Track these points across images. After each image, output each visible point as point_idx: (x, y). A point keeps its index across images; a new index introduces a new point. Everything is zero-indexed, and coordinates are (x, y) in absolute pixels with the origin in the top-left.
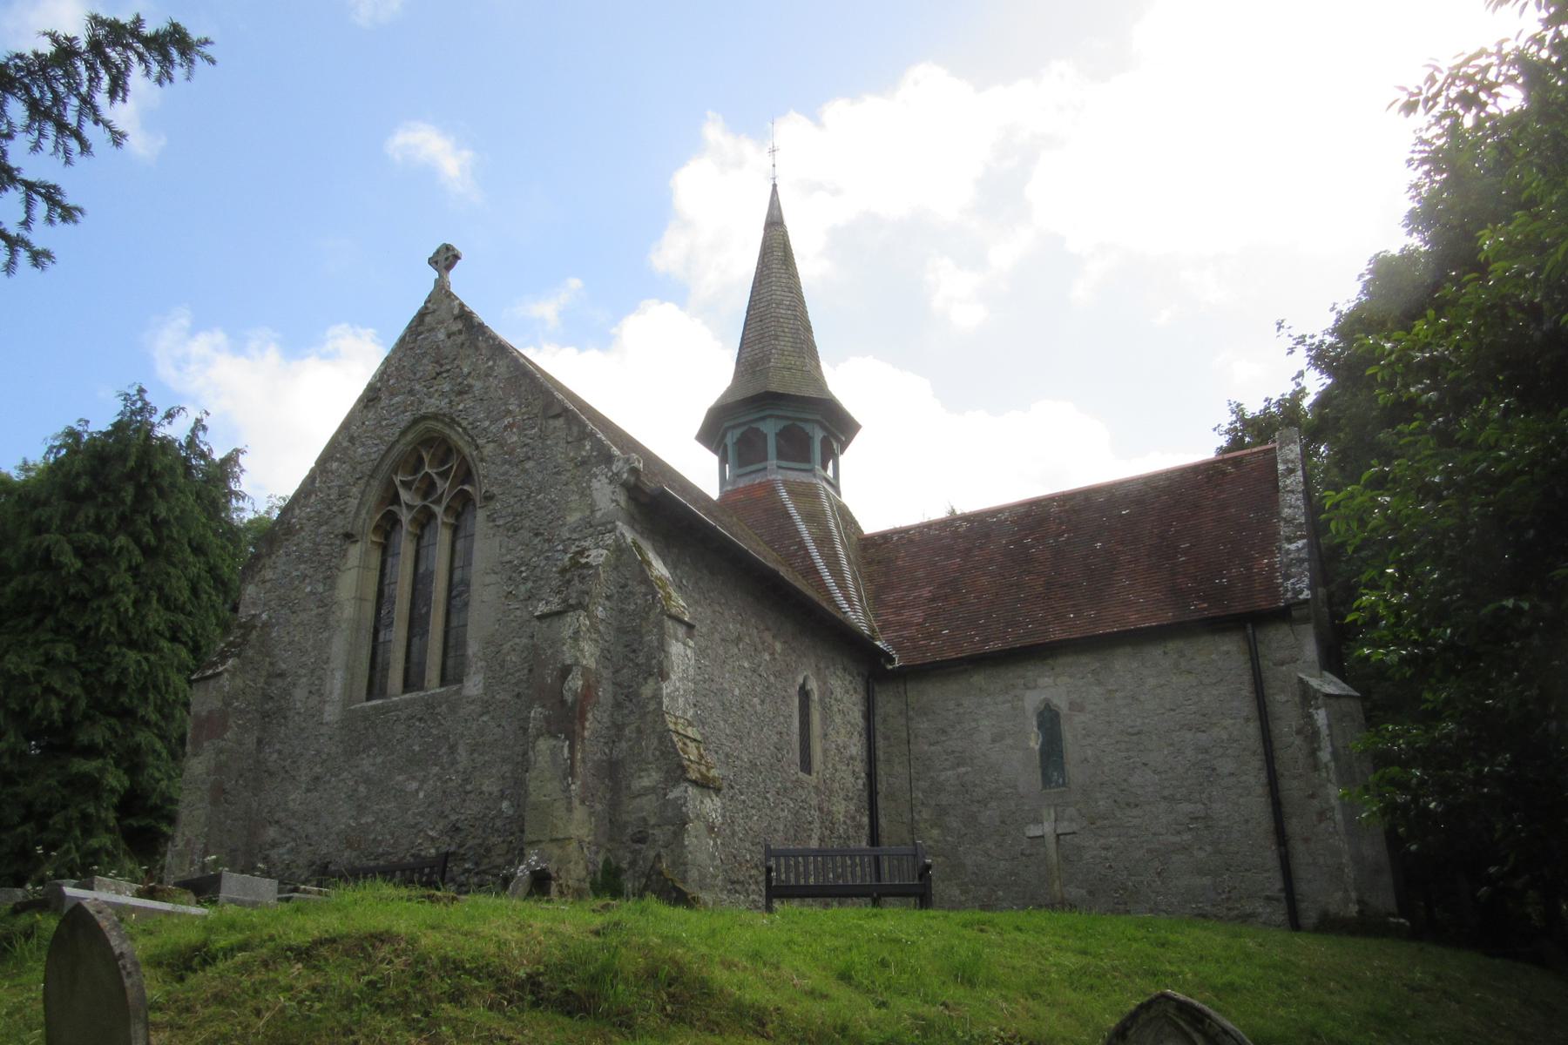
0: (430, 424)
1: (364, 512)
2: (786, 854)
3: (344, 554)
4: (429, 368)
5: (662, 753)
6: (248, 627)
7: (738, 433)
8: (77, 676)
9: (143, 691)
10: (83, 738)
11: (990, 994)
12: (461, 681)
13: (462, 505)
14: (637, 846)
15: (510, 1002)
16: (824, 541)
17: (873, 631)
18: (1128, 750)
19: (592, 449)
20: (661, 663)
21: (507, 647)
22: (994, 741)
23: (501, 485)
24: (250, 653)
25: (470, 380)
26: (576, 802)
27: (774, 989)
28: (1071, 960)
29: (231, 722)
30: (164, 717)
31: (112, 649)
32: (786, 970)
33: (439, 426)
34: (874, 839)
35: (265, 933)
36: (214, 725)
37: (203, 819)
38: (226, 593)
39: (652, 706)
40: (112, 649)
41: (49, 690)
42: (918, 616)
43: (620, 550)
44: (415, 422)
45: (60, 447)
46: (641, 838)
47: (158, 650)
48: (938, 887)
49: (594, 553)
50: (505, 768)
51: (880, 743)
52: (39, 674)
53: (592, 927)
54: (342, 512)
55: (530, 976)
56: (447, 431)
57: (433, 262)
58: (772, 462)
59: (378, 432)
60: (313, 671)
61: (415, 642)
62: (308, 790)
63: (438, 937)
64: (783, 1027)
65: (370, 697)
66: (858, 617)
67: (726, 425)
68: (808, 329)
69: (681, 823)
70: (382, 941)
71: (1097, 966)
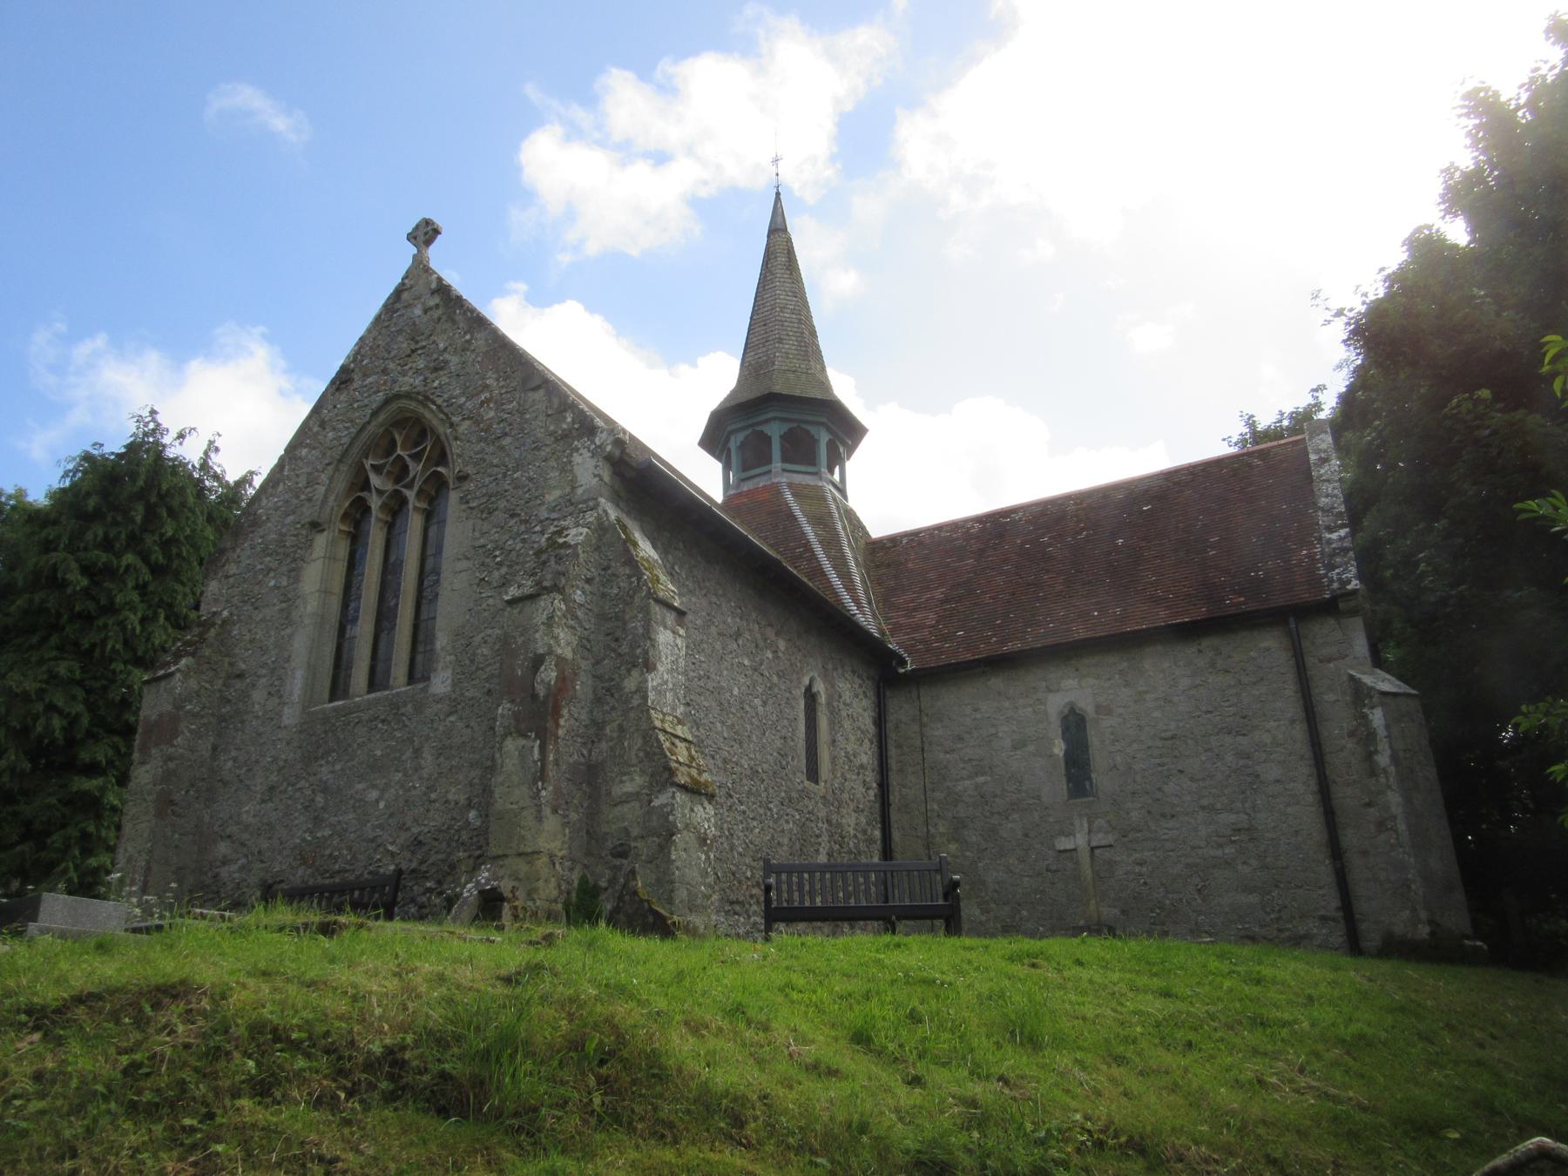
1: (332, 498)
2: (790, 870)
3: (309, 544)
4: (404, 345)
5: (647, 754)
6: (206, 625)
7: (741, 437)
8: (80, 694)
10: (85, 756)
11: (1064, 1060)
12: (428, 679)
13: (435, 489)
14: (617, 862)
15: (350, 1094)
16: (831, 542)
17: (883, 634)
18: (1161, 756)
19: (573, 422)
20: (646, 653)
21: (478, 639)
22: (1015, 748)
23: (476, 464)
24: (207, 652)
25: (447, 356)
26: (547, 811)
27: (760, 1062)
28: (1155, 1007)
29: (183, 726)
31: (118, 666)
32: (780, 1032)
33: (413, 405)
34: (887, 853)
39: (636, 702)
40: (118, 666)
41: (51, 708)
42: (931, 618)
43: (602, 528)
44: (387, 402)
45: (75, 471)
48: (970, 910)
50: (473, 774)
51: (893, 752)
52: (41, 693)
53: (503, 972)
54: (310, 500)
55: (389, 1051)
56: (421, 410)
57: (412, 237)
60: (273, 671)
61: (381, 634)
62: (263, 801)
64: (771, 1128)
66: (867, 619)
67: (729, 428)
68: (813, 334)
69: (667, 834)
70: (175, 997)
71: (1189, 1014)
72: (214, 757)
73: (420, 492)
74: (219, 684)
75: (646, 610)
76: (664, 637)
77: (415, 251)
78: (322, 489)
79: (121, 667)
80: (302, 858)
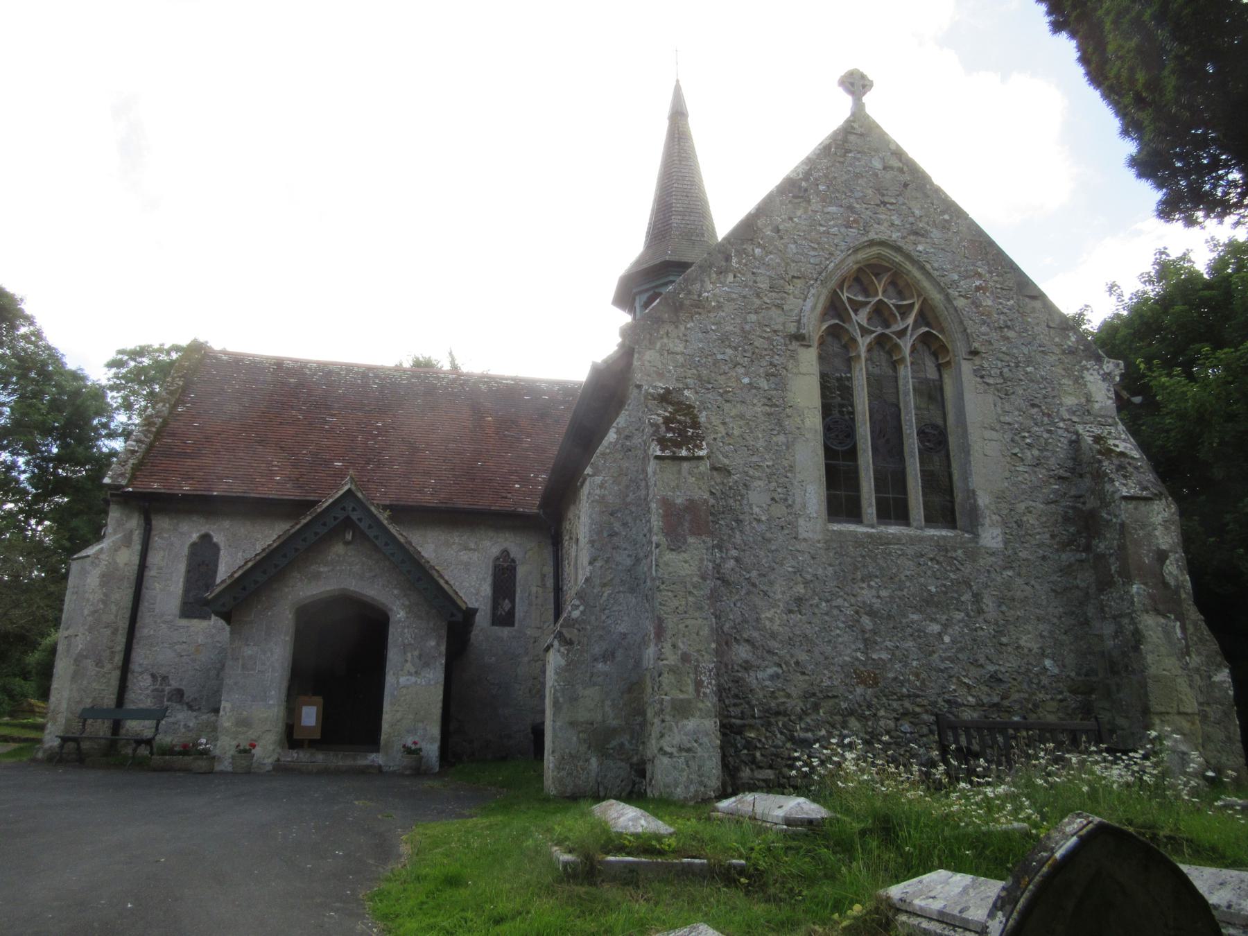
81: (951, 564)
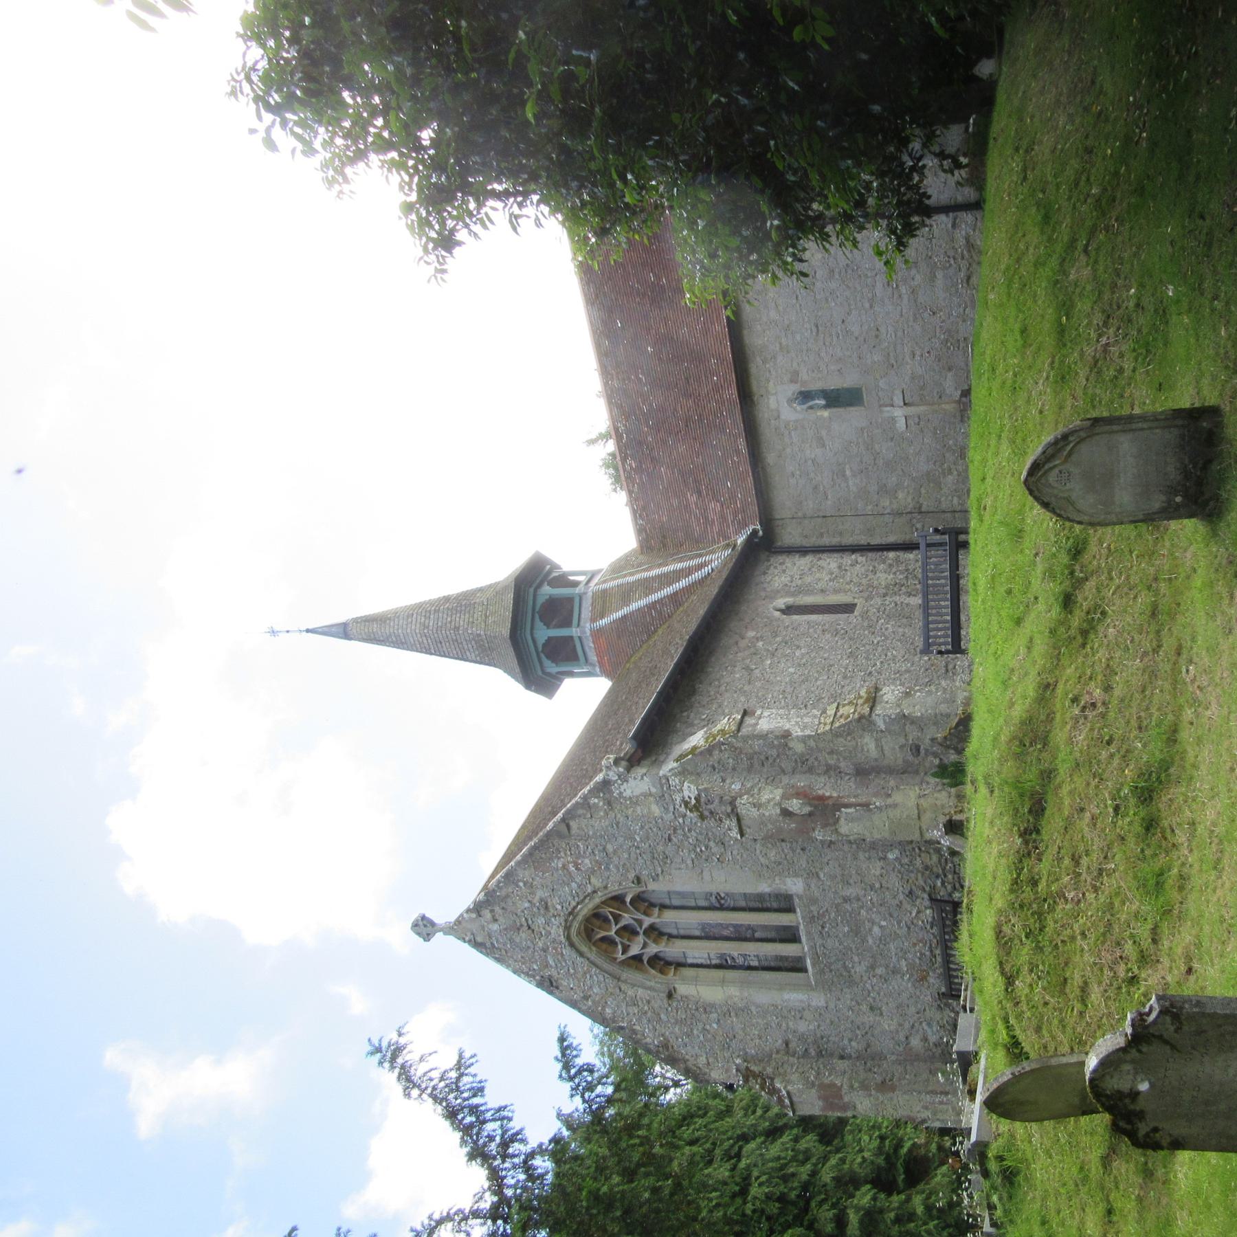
0: (573, 931)
1: (649, 983)
2: (927, 637)
3: (686, 998)
5: (849, 734)
7: (547, 663)
9: (785, 1179)
13: (643, 902)
14: (922, 752)
16: (647, 586)
17: (728, 545)
20: (777, 737)
21: (762, 860)
23: (628, 871)
26: (889, 801)
27: (1026, 674)
29: (826, 1081)
30: (807, 1159)
31: (749, 1208)
34: (910, 547)
35: (996, 1008)
36: (831, 1095)
37: (906, 1097)
38: (692, 1116)
39: (812, 744)
43: (683, 773)
44: (572, 945)
46: (916, 749)
47: (748, 1167)
49: (686, 793)
51: (826, 541)
54: (649, 1002)
55: (1021, 836)
56: (580, 918)
57: (427, 937)
58: (574, 631)
59: (579, 976)
62: (881, 1014)
63: (997, 896)
64: (1051, 671)
65: (803, 970)
67: (540, 673)
68: (447, 599)
72: (850, 1057)
73: (646, 914)
74: (793, 1060)
75: (746, 739)
76: (765, 725)
77: (439, 935)
78: (640, 991)
79: (749, 1206)
80: (922, 980)
81: (823, 915)
